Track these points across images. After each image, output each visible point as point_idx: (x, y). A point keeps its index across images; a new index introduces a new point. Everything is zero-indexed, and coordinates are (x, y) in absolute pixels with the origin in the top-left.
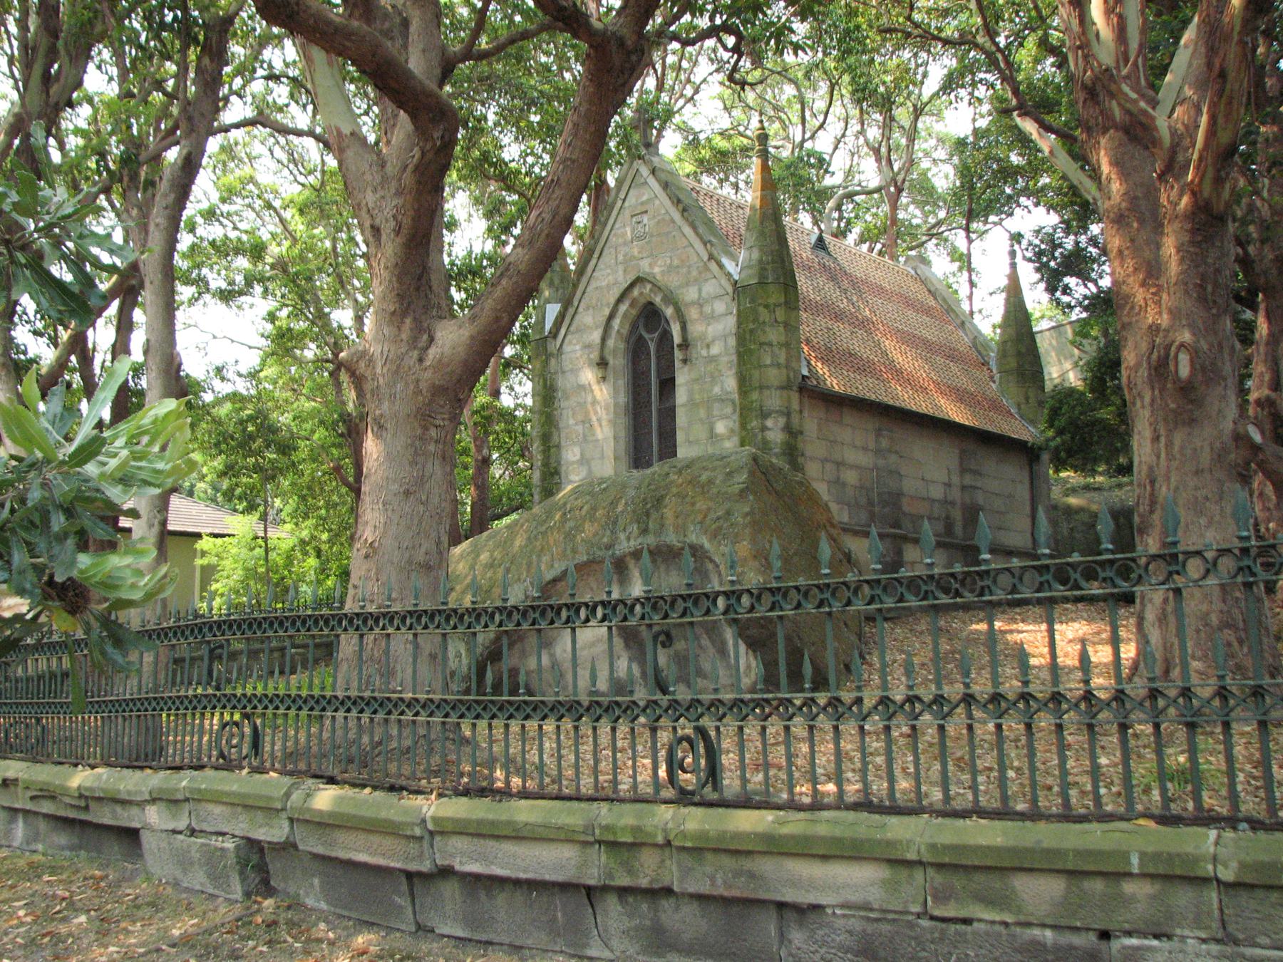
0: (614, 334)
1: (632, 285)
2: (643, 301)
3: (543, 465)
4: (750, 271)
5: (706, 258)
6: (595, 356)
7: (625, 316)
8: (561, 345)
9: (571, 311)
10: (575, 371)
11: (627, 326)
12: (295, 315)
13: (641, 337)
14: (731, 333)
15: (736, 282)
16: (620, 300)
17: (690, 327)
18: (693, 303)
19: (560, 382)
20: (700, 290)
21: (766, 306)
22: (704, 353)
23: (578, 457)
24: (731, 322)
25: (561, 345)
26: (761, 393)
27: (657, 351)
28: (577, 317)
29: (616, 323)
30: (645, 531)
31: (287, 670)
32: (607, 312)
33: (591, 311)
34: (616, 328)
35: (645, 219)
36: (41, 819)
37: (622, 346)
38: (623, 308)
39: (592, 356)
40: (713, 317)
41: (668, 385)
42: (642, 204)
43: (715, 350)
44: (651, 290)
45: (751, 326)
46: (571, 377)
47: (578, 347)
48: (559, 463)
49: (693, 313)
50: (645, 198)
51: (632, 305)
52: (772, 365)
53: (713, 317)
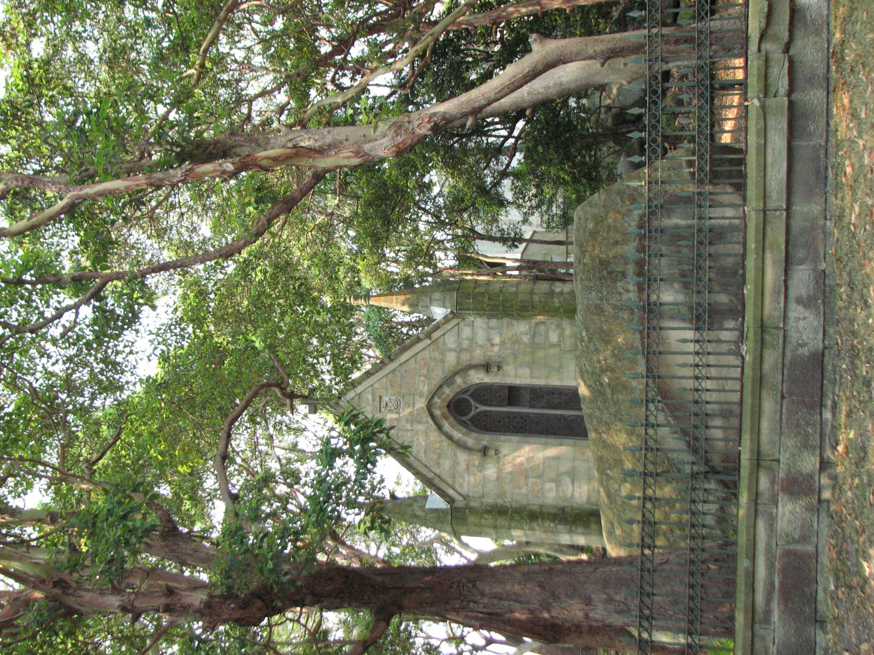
0: (465, 438)
1: (432, 415)
2: (445, 410)
3: (554, 521)
4: (448, 299)
5: (428, 341)
6: (476, 459)
7: (452, 426)
8: (461, 495)
9: (437, 481)
10: (485, 481)
11: (461, 428)
13: (472, 420)
15: (452, 312)
16: (440, 428)
17: (476, 361)
18: (458, 358)
19: (489, 500)
20: (450, 350)
21: (475, 288)
22: (496, 349)
23: (553, 485)
24: (480, 322)
25: (461, 495)
26: (535, 294)
27: (486, 405)
28: (443, 476)
29: (457, 435)
30: (624, 274)
32: (446, 442)
33: (441, 461)
34: (460, 435)
35: (386, 399)
37: (475, 435)
38: (447, 427)
39: (476, 463)
40: (472, 339)
41: (513, 394)
42: (373, 400)
44: (439, 398)
45: (486, 299)
46: (490, 487)
47: (467, 478)
48: (556, 507)
49: (465, 357)
50: (370, 397)
51: (446, 418)
52: (517, 288)
53: (472, 339)
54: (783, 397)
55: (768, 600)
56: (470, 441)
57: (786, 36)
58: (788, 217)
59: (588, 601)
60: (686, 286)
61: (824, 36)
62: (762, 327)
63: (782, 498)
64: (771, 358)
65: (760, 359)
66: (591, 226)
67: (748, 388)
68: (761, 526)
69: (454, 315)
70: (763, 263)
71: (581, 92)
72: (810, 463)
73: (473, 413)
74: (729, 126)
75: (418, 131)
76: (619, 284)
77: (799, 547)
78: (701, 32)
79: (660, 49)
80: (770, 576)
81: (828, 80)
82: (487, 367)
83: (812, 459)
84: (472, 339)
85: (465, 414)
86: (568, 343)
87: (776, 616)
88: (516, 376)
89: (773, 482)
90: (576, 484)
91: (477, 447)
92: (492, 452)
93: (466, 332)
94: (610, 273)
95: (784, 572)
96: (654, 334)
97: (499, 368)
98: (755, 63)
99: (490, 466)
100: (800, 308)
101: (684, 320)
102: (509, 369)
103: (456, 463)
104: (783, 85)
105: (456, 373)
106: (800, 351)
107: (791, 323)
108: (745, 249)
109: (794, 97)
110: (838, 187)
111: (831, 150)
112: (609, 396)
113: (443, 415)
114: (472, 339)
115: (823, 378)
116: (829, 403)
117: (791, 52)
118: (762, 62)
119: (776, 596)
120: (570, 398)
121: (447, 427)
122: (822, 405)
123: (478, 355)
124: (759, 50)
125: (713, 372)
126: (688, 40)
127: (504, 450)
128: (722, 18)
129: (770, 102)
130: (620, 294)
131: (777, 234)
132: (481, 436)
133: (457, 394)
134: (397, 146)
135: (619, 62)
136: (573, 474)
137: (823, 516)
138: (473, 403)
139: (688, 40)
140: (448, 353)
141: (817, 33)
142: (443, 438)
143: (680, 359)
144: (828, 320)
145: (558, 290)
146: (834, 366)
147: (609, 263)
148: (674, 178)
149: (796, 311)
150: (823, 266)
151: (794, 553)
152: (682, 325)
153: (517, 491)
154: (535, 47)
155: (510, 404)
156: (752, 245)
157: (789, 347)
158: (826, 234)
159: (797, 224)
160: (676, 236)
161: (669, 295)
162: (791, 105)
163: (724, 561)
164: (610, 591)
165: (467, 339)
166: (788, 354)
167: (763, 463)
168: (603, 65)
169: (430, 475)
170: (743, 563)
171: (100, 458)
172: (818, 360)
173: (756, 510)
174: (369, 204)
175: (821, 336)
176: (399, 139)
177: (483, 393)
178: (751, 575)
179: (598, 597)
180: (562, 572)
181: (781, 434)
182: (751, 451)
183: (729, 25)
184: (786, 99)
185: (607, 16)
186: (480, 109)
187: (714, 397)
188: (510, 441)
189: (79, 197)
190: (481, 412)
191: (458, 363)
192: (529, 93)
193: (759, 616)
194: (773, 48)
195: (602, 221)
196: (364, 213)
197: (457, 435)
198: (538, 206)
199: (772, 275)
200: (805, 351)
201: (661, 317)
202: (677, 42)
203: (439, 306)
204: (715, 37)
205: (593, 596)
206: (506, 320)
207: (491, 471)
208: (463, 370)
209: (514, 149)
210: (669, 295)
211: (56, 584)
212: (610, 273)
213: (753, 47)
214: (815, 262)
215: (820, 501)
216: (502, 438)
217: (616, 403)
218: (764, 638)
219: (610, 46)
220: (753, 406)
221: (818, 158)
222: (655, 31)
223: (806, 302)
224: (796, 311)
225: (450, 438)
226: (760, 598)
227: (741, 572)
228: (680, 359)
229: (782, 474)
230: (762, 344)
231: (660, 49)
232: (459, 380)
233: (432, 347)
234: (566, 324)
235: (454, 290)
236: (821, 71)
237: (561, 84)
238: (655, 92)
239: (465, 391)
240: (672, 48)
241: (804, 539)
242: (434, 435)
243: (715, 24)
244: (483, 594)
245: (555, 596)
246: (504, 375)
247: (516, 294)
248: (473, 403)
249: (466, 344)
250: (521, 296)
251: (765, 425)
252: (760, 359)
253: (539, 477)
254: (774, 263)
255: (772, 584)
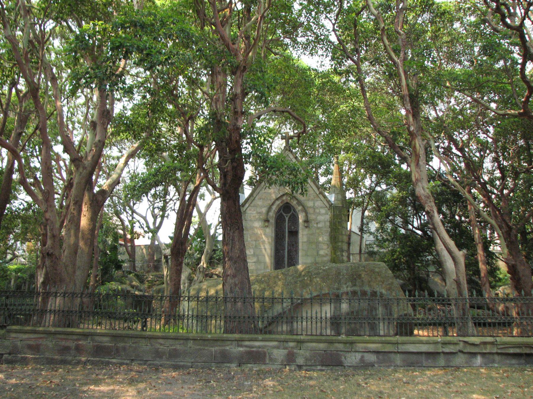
0: (272, 211)
1: (283, 195)
2: (285, 202)
5: (318, 193)
6: (263, 217)
7: (278, 205)
12: (454, 197)
13: (281, 214)
14: (327, 221)
15: (332, 204)
16: (277, 199)
17: (309, 216)
18: (310, 207)
20: (314, 203)
22: (315, 225)
23: (252, 253)
24: (328, 217)
27: (288, 221)
29: (274, 207)
31: (66, 326)
32: (270, 202)
36: (424, 355)
37: (274, 216)
38: (278, 202)
39: (261, 217)
41: (294, 233)
43: (320, 225)
49: (311, 211)
51: (281, 202)
54: (325, 351)
55: (246, 346)
56: (272, 214)
57: (465, 351)
58: (395, 352)
59: (234, 276)
60: (348, 314)
61: (465, 365)
62: (352, 343)
63: (286, 351)
64: (341, 346)
65: (340, 342)
66: (377, 270)
67: (328, 338)
68: (275, 343)
69: (331, 205)
70: (377, 343)
71: (439, 263)
72: (300, 361)
73: (285, 215)
74: (421, 332)
75: (426, 205)
76: (350, 283)
77: (268, 357)
78: (467, 318)
79: (461, 303)
80: (256, 347)
81: (448, 367)
82: (306, 221)
83: (302, 362)
84: (319, 214)
85: (283, 211)
86: (319, 260)
87: (241, 349)
88: (303, 235)
89: (292, 348)
90: (254, 264)
91: (269, 217)
92: (266, 224)
93: (323, 211)
94: (355, 279)
95: (258, 352)
96: (328, 301)
97: (306, 227)
98: (455, 339)
99: (260, 223)
100: (360, 357)
101: (334, 313)
102: (306, 231)
103: (261, 207)
104: (447, 350)
105: (303, 206)
106: (343, 357)
107: (353, 354)
108: (382, 336)
109: (442, 354)
110: (408, 371)
111: (420, 368)
112: (299, 279)
113: (283, 201)
114: (319, 214)
115: (333, 366)
116: (324, 368)
117: (459, 353)
118: (455, 342)
119: (248, 349)
120: (293, 261)
121: (278, 202)
122: (322, 366)
123: (311, 217)
124: (460, 341)
125: (314, 326)
126: (464, 314)
127: (268, 230)
128: (473, 327)
129: (440, 345)
130: (346, 284)
131: (388, 348)
132: (274, 219)
133: (293, 207)
134: (420, 197)
135: (455, 286)
136: (258, 262)
137: (281, 366)
138: (289, 215)
139: (464, 314)
140: (312, 202)
141: (466, 363)
142: (273, 201)
143: (309, 312)
144: (355, 368)
145: (344, 254)
146: (338, 370)
147: (360, 279)
148: (399, 308)
149: (358, 356)
150: (376, 365)
151: (265, 356)
152: (332, 312)
153: (249, 236)
154: (461, 253)
155: (289, 232)
156: (383, 339)
157: (344, 353)
158: (389, 367)
159: (392, 356)
160: (373, 309)
161: (345, 307)
162: (438, 353)
163: (255, 330)
164: (239, 285)
165: (320, 211)
166: (342, 353)
167: (299, 344)
168: (454, 280)
169: (254, 196)
170: (260, 337)
171: (493, 354)
172: (340, 364)
173: (280, 341)
174: (380, 158)
175: (349, 365)
176: (423, 197)
177: (294, 219)
178: (256, 340)
179: (236, 280)
180: (244, 265)
181: (311, 350)
182: (304, 339)
183: (470, 331)
184: (441, 351)
185: (474, 274)
186: (436, 231)
187: (300, 327)
188: (272, 232)
189: (398, 65)
190: (285, 218)
191: (308, 207)
192: (442, 249)
193: (240, 343)
194: (461, 346)
195: (379, 275)
196: (376, 156)
197: (274, 207)
198: (377, 239)
199: (372, 346)
200: (343, 359)
201: (335, 303)
202: (463, 309)
203: (335, 198)
204: (465, 324)
205: (237, 278)
206: (329, 230)
207: (257, 224)
208: (305, 210)
209: (407, 230)
210: (345, 307)
211: (245, 67)
212: (355, 279)
213: (461, 339)
214: (378, 363)
215: (285, 365)
216: (273, 229)
217: (296, 282)
218: (232, 344)
219: (462, 283)
220: (321, 340)
221: (417, 363)
222: (468, 301)
223: (362, 359)
224: (358, 356)
225: (273, 204)
226: (247, 343)
227: (256, 336)
228: (309, 312)
229: (295, 351)
230: (345, 343)
231: (461, 303)
232: (300, 208)
233: (315, 195)
234: (328, 258)
235: (343, 205)
236: (451, 364)
237: (445, 262)
238: (443, 301)
239: (294, 210)
240: (461, 307)
241: (271, 359)
242: (274, 197)
243: (470, 324)
244: (234, 232)
245: (235, 263)
246: (303, 229)
247: (342, 234)
248: (289, 215)
249: (317, 211)
250: (341, 237)
251: (314, 344)
252: (340, 342)
253: (256, 246)
254: (377, 347)
255: (253, 348)
